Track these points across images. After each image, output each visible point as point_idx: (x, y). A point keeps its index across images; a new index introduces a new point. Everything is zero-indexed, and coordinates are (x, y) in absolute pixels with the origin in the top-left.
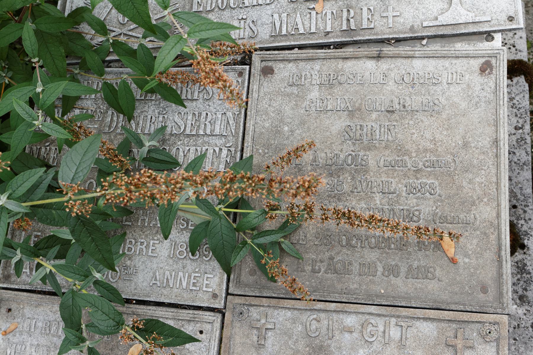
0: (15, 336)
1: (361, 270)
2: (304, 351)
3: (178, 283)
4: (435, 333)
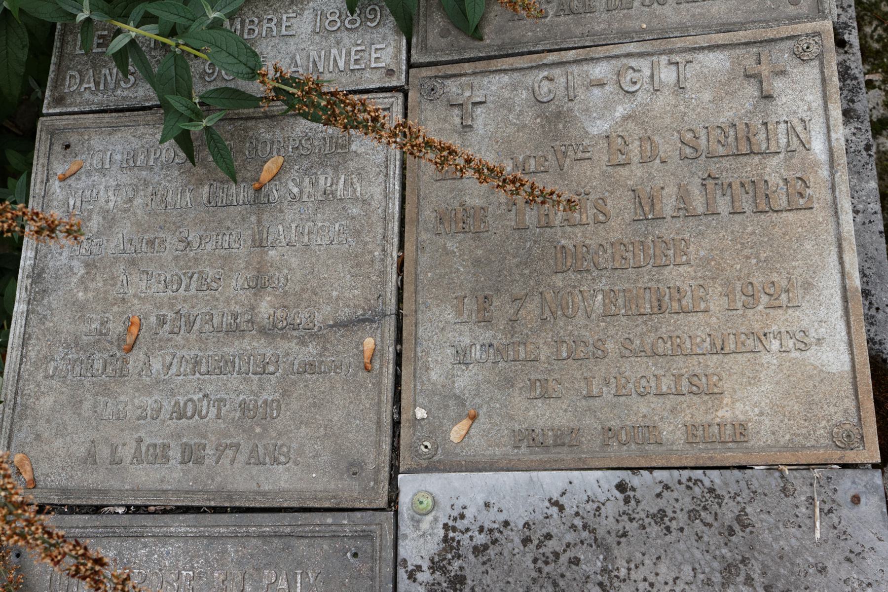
0: (80, 179)
1: (609, 4)
2: (534, 123)
3: (331, 64)
4: (728, 64)
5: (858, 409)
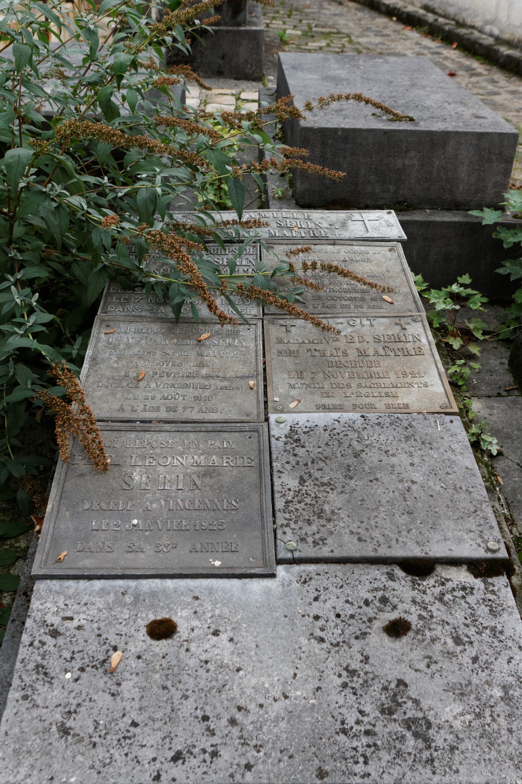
5: (449, 400)
